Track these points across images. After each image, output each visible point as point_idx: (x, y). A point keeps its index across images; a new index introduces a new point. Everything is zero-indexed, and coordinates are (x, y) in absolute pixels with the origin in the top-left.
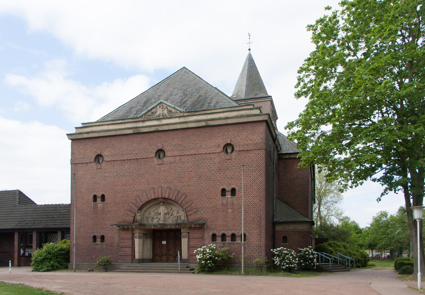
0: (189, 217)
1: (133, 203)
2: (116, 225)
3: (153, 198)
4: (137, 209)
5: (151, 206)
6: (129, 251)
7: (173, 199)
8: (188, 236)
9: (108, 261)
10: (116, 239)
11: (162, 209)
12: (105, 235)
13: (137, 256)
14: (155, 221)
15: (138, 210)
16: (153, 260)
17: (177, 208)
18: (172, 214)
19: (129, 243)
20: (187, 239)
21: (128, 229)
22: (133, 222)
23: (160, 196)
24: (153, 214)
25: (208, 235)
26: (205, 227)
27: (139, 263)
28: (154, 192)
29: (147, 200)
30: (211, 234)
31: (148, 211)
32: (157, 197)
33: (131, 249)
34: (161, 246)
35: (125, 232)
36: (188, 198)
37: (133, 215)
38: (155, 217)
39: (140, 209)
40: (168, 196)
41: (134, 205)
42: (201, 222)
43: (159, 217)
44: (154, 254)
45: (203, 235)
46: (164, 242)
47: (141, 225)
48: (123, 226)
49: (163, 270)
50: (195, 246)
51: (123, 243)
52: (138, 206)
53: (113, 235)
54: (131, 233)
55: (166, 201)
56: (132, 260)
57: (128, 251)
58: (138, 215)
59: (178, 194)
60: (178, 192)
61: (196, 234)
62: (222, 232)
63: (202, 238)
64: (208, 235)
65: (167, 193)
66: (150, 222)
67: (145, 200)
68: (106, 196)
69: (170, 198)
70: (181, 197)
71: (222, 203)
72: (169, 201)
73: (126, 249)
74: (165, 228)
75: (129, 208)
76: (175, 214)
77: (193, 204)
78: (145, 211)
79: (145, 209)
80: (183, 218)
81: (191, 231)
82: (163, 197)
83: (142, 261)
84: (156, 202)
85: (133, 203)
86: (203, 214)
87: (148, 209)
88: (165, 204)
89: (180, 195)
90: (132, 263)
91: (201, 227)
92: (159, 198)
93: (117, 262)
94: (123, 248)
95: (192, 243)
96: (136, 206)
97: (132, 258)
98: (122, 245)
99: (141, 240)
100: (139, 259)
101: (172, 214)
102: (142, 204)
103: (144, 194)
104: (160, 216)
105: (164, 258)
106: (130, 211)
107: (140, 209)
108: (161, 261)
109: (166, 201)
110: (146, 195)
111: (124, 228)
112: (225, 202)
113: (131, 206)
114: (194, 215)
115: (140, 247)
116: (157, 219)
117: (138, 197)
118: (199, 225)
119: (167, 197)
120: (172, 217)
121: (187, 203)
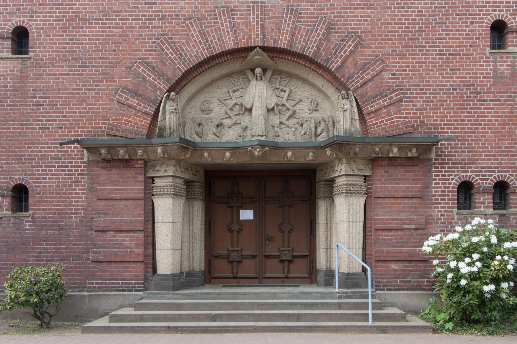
0: (370, 121)
1: (147, 64)
2: (77, 141)
3: (230, 46)
4: (164, 86)
5: (213, 81)
6: (132, 244)
7: (310, 52)
8: (364, 188)
9: (54, 286)
10: (80, 200)
11: (258, 93)
12: (31, 185)
13: (166, 263)
14: (230, 136)
15: (169, 91)
16: (209, 276)
17: (314, 92)
18: (294, 113)
19: (133, 214)
20: (361, 201)
21: (127, 163)
22: (150, 134)
23: (257, 41)
24: (218, 110)
25: (443, 186)
26: (433, 156)
27: (174, 288)
28: (233, 26)
29: (206, 54)
30: (454, 182)
31: (198, 102)
32: (243, 44)
33: (141, 235)
34: (235, 227)
35: (115, 171)
36: (368, 52)
37: (151, 110)
38: (227, 122)
39: (177, 86)
40: (291, 42)
41: (153, 70)
42: (419, 135)
43: (245, 120)
44: (211, 256)
45: (427, 186)
46: (247, 215)
47: (186, 145)
48: (111, 148)
49: (298, 318)
50: (394, 225)
51: (106, 214)
52: (170, 74)
53: (64, 184)
54: (141, 178)
55: (276, 60)
56: (146, 279)
57: (127, 243)
58: (170, 107)
59: (327, 37)
60: (330, 28)
61: (395, 182)
62: (496, 176)
63: (422, 196)
64: (443, 186)
65: (286, 29)
66: (210, 138)
67: (197, 52)
68: (33, 35)
69: (297, 48)
70: (338, 48)
71: (495, 71)
72: (284, 65)
73: (120, 237)
74: (275, 159)
75: (130, 82)
76: (303, 111)
77: (386, 75)
78: (190, 99)
79: (190, 89)
80: (347, 125)
81: (380, 172)
82: (270, 44)
83: (183, 280)
84: (236, 65)
85: (147, 64)
86: (421, 114)
87: (200, 90)
88: (269, 74)
89: (335, 38)
90: (146, 289)
91: (417, 154)
92: (250, 49)
93: (81, 287)
94: (109, 235)
95: (382, 214)
96: (162, 75)
97: (146, 272)
98: (102, 221)
99: (181, 203)
100: (175, 277)
101: (294, 113)
102: (184, 69)
103: (194, 31)
104: (251, 117)
105: (248, 268)
106: (136, 94)
107: (177, 86)
108: (236, 279)
109: (276, 60)
110: (203, 34)
111: (111, 155)
112: (504, 68)
113: (138, 75)
114: (388, 114)
115: (174, 230)
116: (238, 130)
117: (170, 41)
118: (417, 146)
119: (283, 44)
120: (293, 121)
121: (364, 67)
